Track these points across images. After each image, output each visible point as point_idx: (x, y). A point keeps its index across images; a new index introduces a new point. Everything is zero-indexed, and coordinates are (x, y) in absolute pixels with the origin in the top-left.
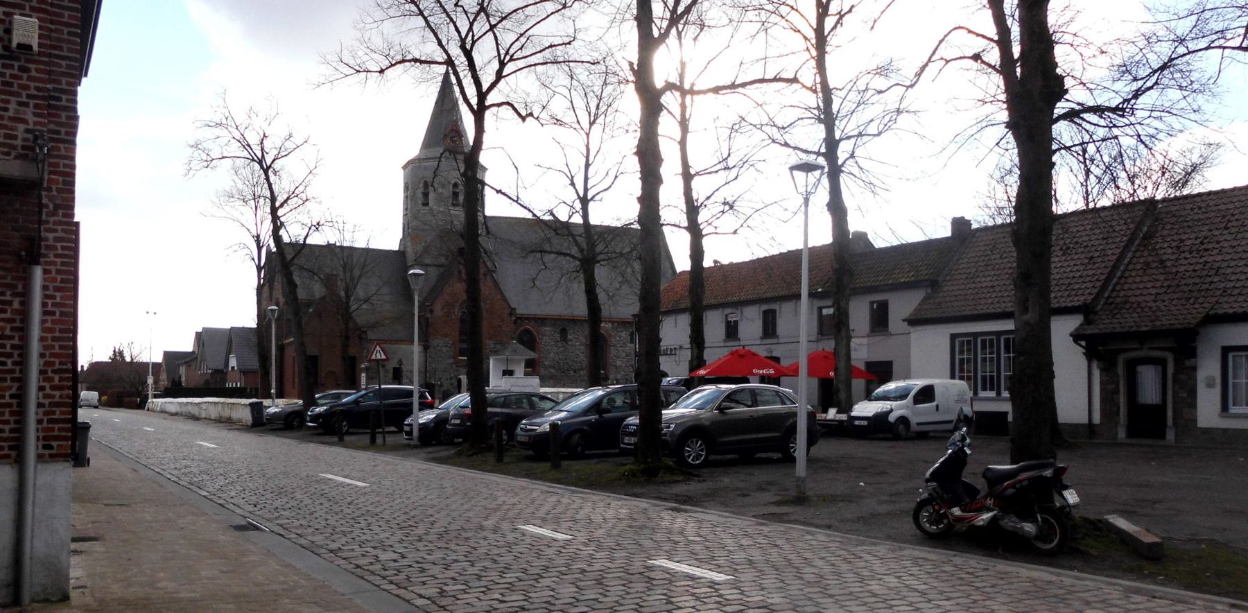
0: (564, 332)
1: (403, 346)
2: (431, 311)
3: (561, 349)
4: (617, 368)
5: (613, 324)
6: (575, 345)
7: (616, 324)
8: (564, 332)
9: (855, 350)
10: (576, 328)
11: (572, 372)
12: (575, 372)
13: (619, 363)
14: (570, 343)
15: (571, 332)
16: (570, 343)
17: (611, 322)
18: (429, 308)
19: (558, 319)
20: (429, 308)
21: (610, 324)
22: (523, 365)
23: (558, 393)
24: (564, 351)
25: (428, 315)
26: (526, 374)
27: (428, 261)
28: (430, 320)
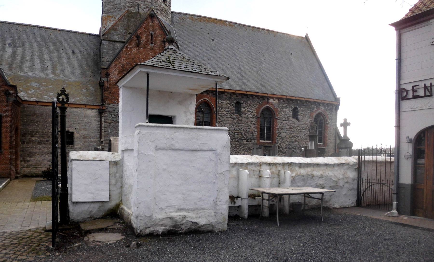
0: (238, 105)
1: (76, 110)
2: (107, 75)
3: (235, 121)
4: (282, 138)
5: (279, 101)
6: (247, 118)
7: (282, 101)
8: (238, 105)
9: (108, 173)
10: (249, 102)
11: (245, 141)
12: (247, 141)
13: (283, 134)
14: (243, 115)
15: (245, 105)
16: (243, 115)
17: (277, 98)
18: (105, 71)
19: (233, 93)
20: (105, 71)
21: (277, 100)
22: (193, 108)
23: (260, 164)
24: (238, 122)
25: (104, 79)
26: (198, 122)
27: (116, 38)
28: (106, 84)
